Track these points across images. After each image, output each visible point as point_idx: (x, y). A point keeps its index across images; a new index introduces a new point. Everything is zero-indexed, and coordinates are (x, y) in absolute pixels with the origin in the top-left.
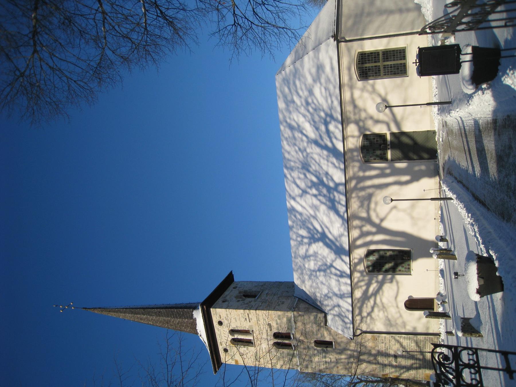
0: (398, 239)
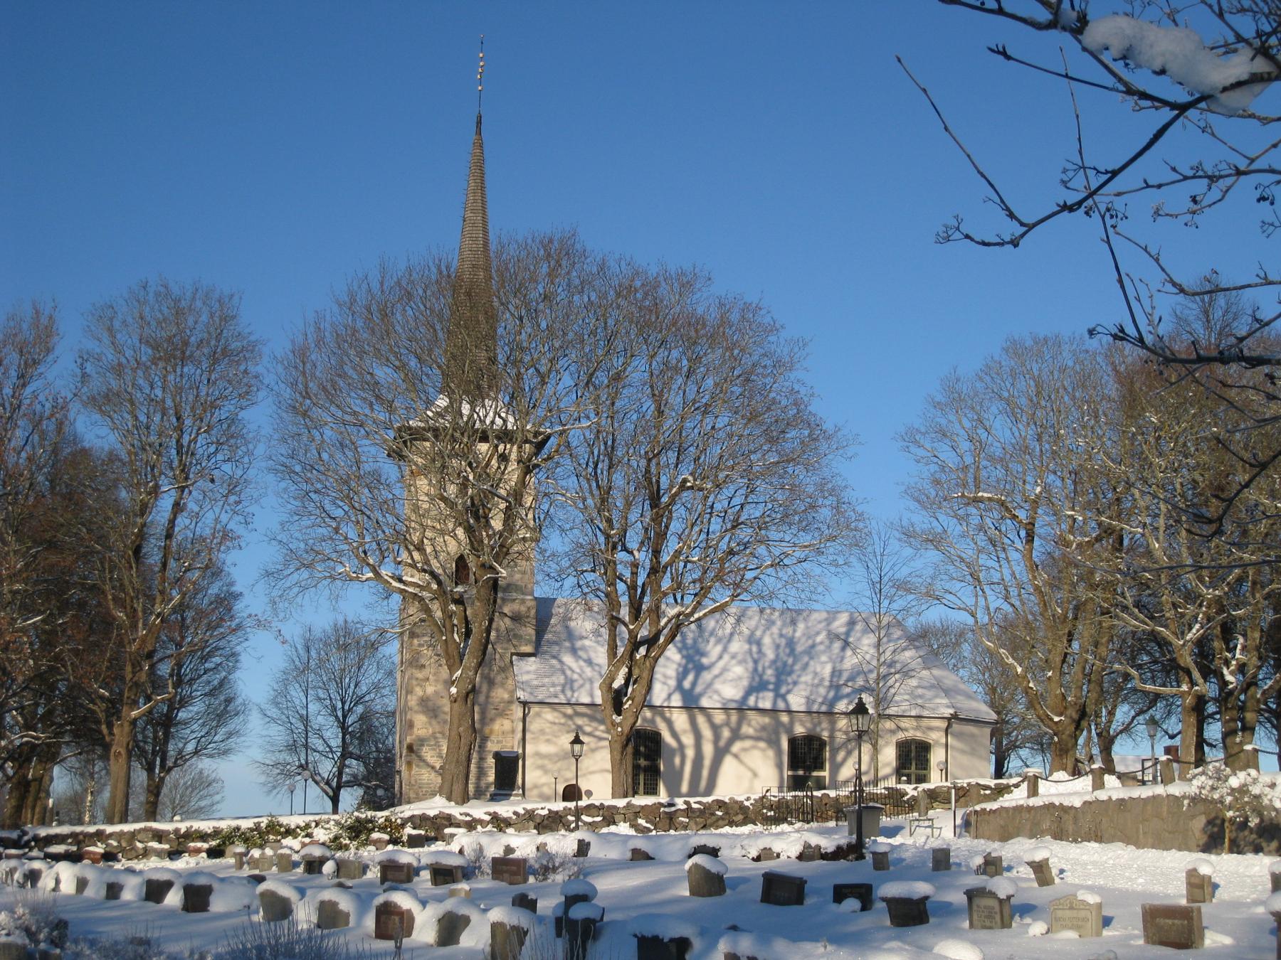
0: (705, 773)
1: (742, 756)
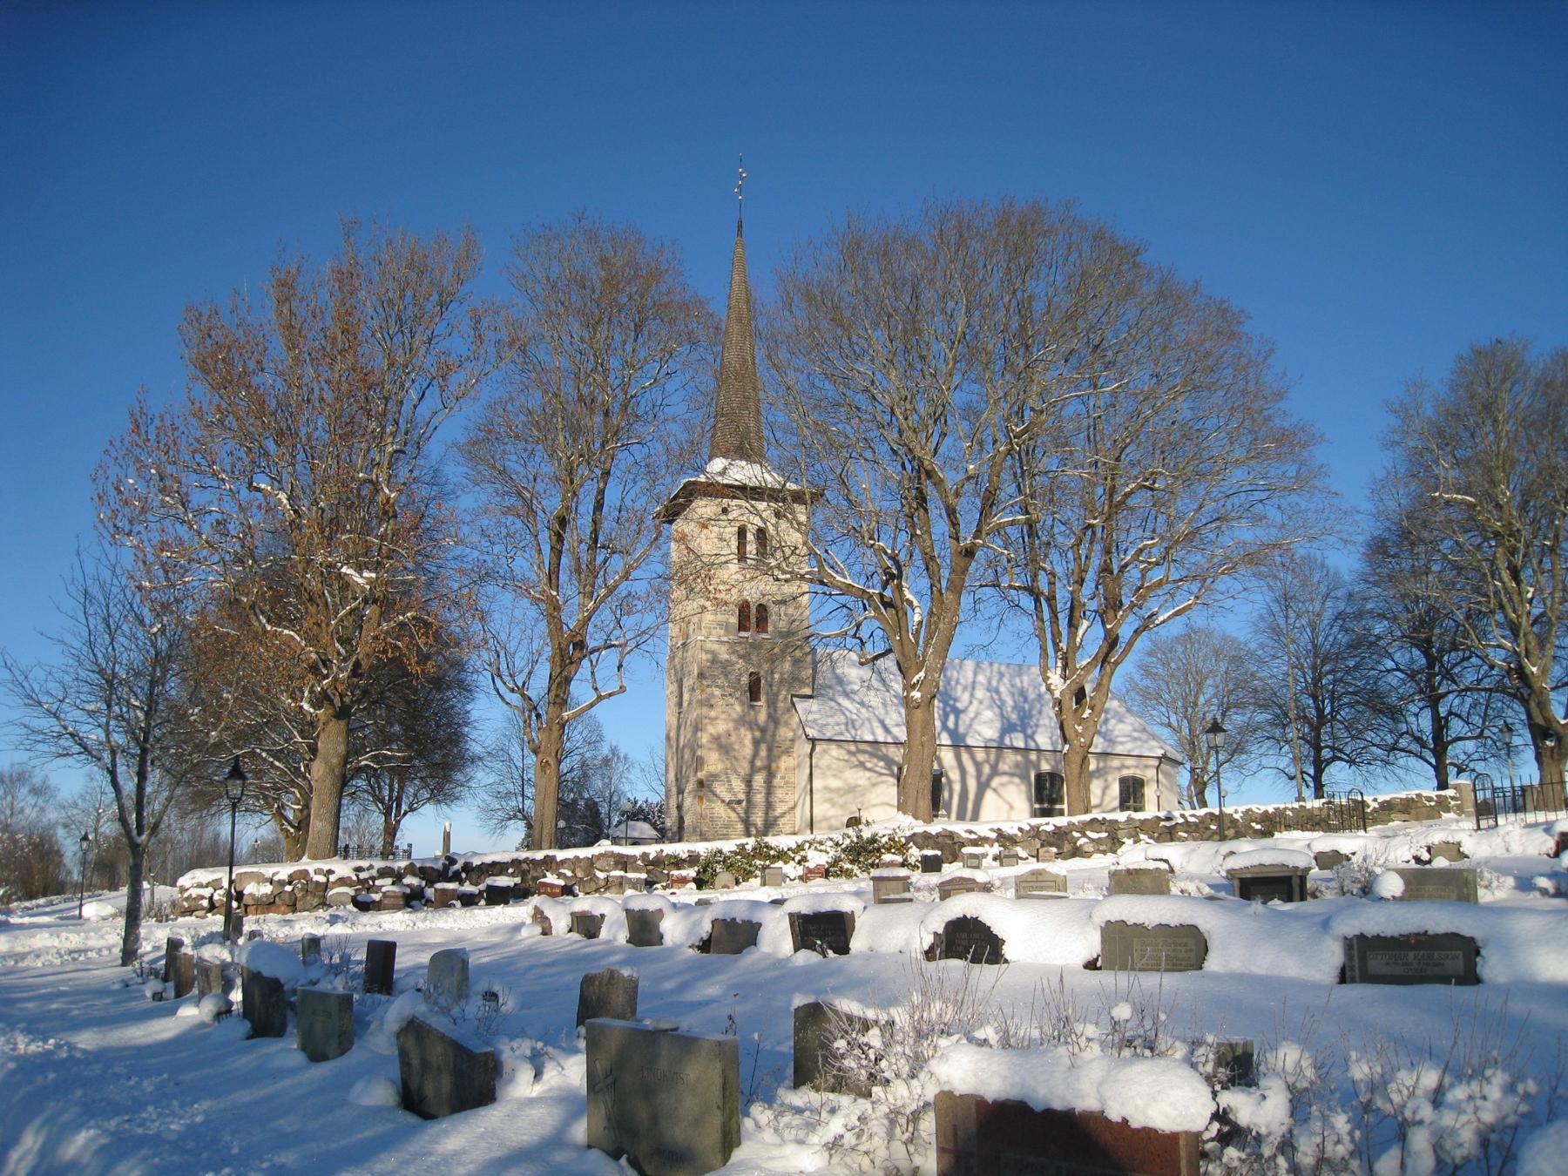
0: (970, 806)
1: (1001, 790)
